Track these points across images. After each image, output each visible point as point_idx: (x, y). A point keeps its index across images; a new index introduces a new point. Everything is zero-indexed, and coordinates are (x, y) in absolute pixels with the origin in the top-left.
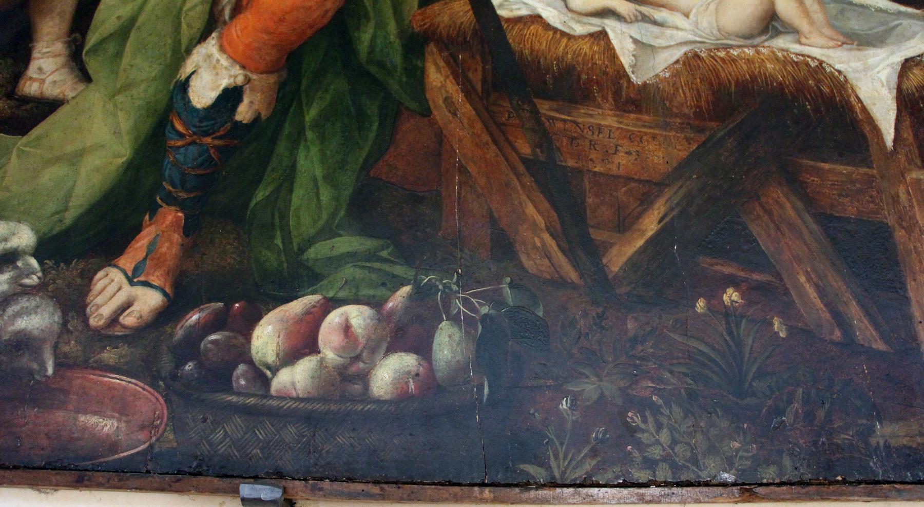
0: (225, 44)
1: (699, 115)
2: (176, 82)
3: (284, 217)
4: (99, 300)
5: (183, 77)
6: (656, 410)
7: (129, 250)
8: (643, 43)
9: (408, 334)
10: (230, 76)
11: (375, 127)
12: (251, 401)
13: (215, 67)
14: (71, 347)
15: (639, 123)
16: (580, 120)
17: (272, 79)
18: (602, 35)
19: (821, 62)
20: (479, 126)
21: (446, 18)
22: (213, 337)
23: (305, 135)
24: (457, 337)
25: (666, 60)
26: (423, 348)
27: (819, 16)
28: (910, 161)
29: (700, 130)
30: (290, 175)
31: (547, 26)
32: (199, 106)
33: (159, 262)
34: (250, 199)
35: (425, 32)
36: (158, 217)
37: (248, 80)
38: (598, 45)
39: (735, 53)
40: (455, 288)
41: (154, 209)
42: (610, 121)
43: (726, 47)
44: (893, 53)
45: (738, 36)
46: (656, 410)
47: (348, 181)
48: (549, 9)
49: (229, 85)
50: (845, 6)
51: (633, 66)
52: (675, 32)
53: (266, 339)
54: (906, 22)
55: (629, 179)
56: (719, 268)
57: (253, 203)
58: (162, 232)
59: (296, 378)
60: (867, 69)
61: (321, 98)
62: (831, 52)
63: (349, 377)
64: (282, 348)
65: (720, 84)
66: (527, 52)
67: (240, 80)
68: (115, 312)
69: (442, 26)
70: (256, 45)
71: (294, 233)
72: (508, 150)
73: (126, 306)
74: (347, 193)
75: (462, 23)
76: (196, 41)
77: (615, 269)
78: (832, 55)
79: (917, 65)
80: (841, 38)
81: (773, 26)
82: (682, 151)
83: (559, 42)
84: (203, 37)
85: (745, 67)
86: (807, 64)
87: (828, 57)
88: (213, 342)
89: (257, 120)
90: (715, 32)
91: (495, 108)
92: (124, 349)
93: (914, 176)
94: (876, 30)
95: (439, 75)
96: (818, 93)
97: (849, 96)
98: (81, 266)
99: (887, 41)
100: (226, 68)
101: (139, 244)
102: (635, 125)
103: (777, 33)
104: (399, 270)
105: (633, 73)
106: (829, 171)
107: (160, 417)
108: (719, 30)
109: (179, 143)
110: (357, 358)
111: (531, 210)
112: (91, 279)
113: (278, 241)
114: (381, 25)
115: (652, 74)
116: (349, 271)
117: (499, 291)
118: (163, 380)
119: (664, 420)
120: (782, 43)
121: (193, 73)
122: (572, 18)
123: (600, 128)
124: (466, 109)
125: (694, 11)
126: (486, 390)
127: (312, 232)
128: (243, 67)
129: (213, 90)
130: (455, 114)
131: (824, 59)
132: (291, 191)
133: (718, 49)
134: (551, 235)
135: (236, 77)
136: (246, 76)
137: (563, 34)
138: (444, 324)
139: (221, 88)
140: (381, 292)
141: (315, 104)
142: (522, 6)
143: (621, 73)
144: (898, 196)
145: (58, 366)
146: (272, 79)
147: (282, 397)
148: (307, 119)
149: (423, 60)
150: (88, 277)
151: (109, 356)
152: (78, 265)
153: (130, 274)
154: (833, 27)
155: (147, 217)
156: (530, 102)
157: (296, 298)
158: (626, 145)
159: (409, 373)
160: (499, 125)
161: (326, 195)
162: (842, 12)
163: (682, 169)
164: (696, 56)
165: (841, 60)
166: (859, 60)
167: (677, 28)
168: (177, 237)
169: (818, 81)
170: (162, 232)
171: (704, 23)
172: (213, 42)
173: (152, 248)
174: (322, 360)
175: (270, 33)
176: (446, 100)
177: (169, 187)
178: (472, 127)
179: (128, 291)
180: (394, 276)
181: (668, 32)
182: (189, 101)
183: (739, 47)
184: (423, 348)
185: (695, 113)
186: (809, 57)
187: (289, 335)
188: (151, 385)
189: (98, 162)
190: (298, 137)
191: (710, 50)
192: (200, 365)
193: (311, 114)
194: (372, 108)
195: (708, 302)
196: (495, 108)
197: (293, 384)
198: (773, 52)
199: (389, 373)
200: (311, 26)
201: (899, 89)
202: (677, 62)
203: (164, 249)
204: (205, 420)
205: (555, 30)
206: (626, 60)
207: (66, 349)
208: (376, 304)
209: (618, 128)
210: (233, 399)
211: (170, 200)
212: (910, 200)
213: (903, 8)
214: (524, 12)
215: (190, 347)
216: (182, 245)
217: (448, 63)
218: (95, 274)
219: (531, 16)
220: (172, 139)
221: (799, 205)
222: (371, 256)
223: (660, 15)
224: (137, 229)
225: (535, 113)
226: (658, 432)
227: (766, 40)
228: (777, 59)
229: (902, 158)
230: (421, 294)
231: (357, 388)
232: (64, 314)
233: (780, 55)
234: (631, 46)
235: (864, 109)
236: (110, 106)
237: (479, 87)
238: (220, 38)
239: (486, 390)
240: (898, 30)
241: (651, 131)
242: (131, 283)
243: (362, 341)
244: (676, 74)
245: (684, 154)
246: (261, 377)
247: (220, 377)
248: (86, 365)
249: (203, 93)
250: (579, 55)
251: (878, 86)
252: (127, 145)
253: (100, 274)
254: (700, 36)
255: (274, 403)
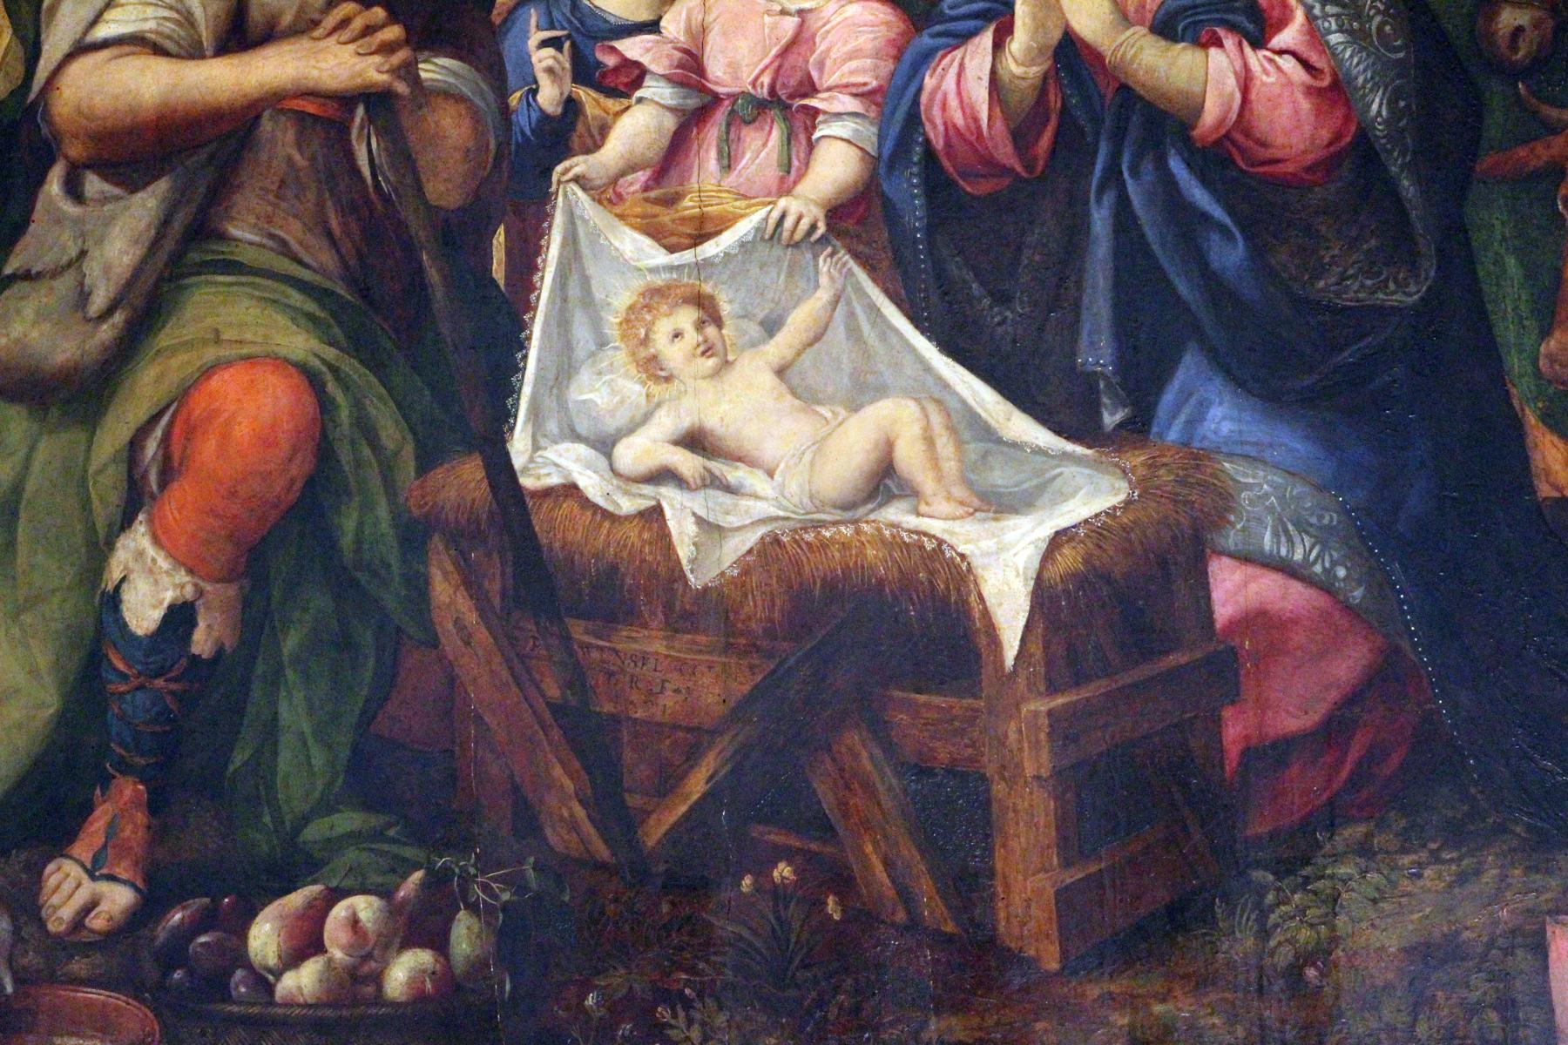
0: (159, 532)
1: (770, 633)
2: (103, 593)
3: (271, 787)
4: (55, 900)
5: (110, 588)
6: (688, 1005)
7: (82, 835)
8: (709, 523)
9: (421, 926)
10: (175, 586)
11: (371, 662)
12: (256, 1010)
13: (151, 571)
14: (31, 959)
15: (695, 647)
16: (619, 647)
17: (231, 591)
18: (655, 514)
19: (941, 542)
20: (497, 659)
21: (453, 494)
22: (203, 939)
23: (412, 845)
24: (476, 928)
25: (737, 549)
26: (439, 942)
27: (950, 466)
28: (1030, 686)
29: (770, 655)
30: (271, 730)
31: (586, 503)
32: (140, 632)
33: (123, 850)
34: (226, 766)
35: (426, 516)
36: (113, 789)
37: (200, 593)
38: (650, 529)
39: (828, 534)
40: (472, 871)
41: (105, 781)
42: (659, 647)
43: (819, 525)
44: (1041, 522)
45: (835, 506)
46: (688, 1005)
47: (344, 740)
48: (589, 473)
49: (176, 599)
50: (990, 445)
51: (692, 561)
52: (751, 503)
53: (264, 937)
54: (1069, 470)
55: (675, 727)
56: (772, 837)
57: (231, 768)
58: (118, 809)
59: (302, 981)
60: (1002, 549)
61: (300, 621)
62: (957, 526)
63: (359, 979)
64: (284, 947)
65: (801, 584)
66: (557, 545)
67: (189, 592)
68: (78, 913)
69: (448, 507)
70: (202, 534)
71: (285, 809)
72: (533, 692)
73: (91, 906)
74: (344, 753)
75: (474, 500)
76: (116, 528)
77: (650, 843)
78: (957, 530)
79: (1071, 540)
80: (976, 502)
81: (886, 486)
82: (743, 686)
83: (600, 526)
84: (126, 522)
85: (837, 555)
86: (922, 547)
87: (952, 533)
88: (202, 944)
89: (220, 652)
90: (806, 500)
91: (517, 633)
92: (98, 958)
93: (1032, 708)
94: (1026, 486)
95: (445, 585)
96: (928, 592)
97: (969, 594)
98: (23, 857)
99: (1039, 503)
100: (167, 572)
101: (93, 829)
102: (690, 651)
103: (890, 497)
104: (409, 852)
105: (692, 571)
106: (925, 705)
107: (151, 1034)
108: (811, 497)
109: (123, 688)
110: (368, 957)
111: (558, 771)
112: (40, 873)
113: (267, 819)
114: (367, 507)
115: (715, 572)
116: (351, 855)
117: (522, 873)
118: (149, 990)
119: (697, 1016)
120: (896, 514)
121: (123, 580)
122: (619, 487)
123: (644, 658)
124: (482, 635)
125: (782, 466)
126: (508, 987)
127: (307, 808)
128: (190, 571)
129: (154, 607)
130: (468, 644)
131: (946, 537)
132: (275, 753)
133: (805, 529)
134: (580, 801)
135: (182, 586)
136: (196, 585)
137: (606, 514)
138: (462, 915)
139: (166, 604)
140: (390, 879)
141: (292, 632)
142: (553, 469)
143: (676, 574)
144: (1006, 736)
145: (17, 981)
146: (231, 591)
147: (289, 1004)
148: (285, 651)
149: (426, 563)
150: (36, 873)
151: (79, 966)
152: (20, 857)
153: (89, 866)
154: (967, 483)
155: (98, 792)
156: (561, 620)
157: (295, 889)
158: (675, 681)
159: (424, 971)
160: (522, 658)
161: (319, 758)
162: (985, 455)
163: (739, 712)
164: (776, 541)
165: (969, 538)
166: (994, 536)
167: (757, 497)
168: (141, 818)
169: (932, 573)
170: (118, 809)
171: (793, 487)
172: (142, 529)
173: (112, 829)
174: (330, 960)
175: (217, 516)
176: (457, 621)
177: (119, 750)
178: (489, 662)
179: (88, 889)
180: (404, 860)
181: (745, 503)
182: (125, 625)
183: (835, 523)
184: (439, 942)
185: (765, 630)
186: (925, 534)
187: (291, 936)
188: (135, 998)
189: (16, 715)
190: (275, 679)
191: (795, 531)
192: (191, 973)
193: (291, 643)
194: (366, 638)
195: (756, 881)
196: (517, 633)
197: (300, 988)
198: (879, 530)
199: (404, 971)
200: (276, 506)
201: (1039, 579)
202: (750, 552)
203: (127, 833)
204: (203, 1034)
205: (596, 508)
206: (684, 552)
207: (25, 961)
208: (385, 893)
209: (666, 656)
210: (235, 1009)
211: (125, 768)
212: (1020, 741)
213: (1070, 447)
214: (555, 480)
215: (175, 952)
216: (149, 827)
217: (456, 564)
218: (45, 866)
219: (564, 486)
220: (110, 682)
221: (877, 752)
222: (378, 835)
223: (735, 474)
224: (86, 809)
225: (567, 638)
226: (688, 1028)
227: (872, 511)
228: (883, 541)
229: (1021, 681)
230: (437, 881)
231: (370, 990)
232: (14, 919)
233: (887, 533)
234: (691, 528)
235: (986, 613)
236: (16, 631)
237: (497, 601)
238: (150, 521)
239: (508, 987)
240: (1058, 483)
241: (707, 657)
242: (93, 878)
243: (372, 938)
244: (746, 572)
245: (746, 688)
246: (263, 983)
247: (218, 985)
248: (52, 979)
249: (143, 610)
250: (625, 546)
251: (1011, 575)
252: (53, 691)
253: (51, 867)
254: (786, 509)
255: (280, 1011)
